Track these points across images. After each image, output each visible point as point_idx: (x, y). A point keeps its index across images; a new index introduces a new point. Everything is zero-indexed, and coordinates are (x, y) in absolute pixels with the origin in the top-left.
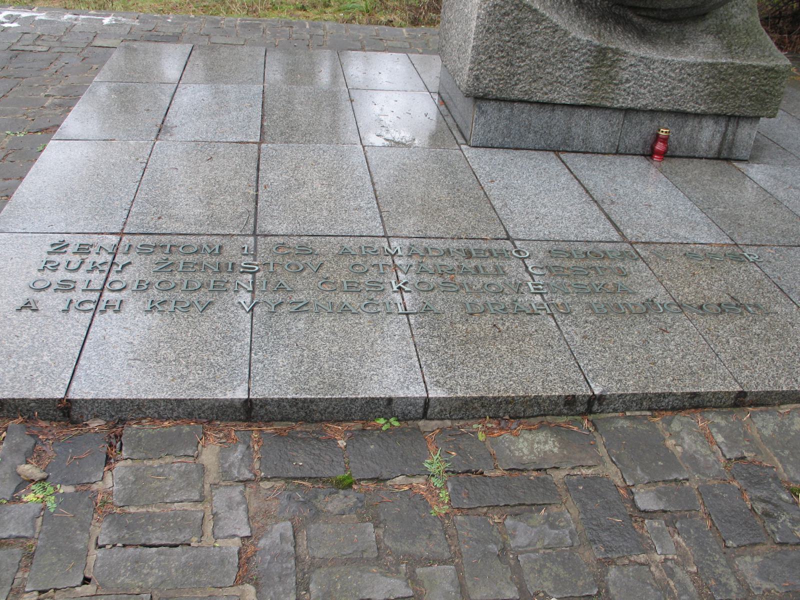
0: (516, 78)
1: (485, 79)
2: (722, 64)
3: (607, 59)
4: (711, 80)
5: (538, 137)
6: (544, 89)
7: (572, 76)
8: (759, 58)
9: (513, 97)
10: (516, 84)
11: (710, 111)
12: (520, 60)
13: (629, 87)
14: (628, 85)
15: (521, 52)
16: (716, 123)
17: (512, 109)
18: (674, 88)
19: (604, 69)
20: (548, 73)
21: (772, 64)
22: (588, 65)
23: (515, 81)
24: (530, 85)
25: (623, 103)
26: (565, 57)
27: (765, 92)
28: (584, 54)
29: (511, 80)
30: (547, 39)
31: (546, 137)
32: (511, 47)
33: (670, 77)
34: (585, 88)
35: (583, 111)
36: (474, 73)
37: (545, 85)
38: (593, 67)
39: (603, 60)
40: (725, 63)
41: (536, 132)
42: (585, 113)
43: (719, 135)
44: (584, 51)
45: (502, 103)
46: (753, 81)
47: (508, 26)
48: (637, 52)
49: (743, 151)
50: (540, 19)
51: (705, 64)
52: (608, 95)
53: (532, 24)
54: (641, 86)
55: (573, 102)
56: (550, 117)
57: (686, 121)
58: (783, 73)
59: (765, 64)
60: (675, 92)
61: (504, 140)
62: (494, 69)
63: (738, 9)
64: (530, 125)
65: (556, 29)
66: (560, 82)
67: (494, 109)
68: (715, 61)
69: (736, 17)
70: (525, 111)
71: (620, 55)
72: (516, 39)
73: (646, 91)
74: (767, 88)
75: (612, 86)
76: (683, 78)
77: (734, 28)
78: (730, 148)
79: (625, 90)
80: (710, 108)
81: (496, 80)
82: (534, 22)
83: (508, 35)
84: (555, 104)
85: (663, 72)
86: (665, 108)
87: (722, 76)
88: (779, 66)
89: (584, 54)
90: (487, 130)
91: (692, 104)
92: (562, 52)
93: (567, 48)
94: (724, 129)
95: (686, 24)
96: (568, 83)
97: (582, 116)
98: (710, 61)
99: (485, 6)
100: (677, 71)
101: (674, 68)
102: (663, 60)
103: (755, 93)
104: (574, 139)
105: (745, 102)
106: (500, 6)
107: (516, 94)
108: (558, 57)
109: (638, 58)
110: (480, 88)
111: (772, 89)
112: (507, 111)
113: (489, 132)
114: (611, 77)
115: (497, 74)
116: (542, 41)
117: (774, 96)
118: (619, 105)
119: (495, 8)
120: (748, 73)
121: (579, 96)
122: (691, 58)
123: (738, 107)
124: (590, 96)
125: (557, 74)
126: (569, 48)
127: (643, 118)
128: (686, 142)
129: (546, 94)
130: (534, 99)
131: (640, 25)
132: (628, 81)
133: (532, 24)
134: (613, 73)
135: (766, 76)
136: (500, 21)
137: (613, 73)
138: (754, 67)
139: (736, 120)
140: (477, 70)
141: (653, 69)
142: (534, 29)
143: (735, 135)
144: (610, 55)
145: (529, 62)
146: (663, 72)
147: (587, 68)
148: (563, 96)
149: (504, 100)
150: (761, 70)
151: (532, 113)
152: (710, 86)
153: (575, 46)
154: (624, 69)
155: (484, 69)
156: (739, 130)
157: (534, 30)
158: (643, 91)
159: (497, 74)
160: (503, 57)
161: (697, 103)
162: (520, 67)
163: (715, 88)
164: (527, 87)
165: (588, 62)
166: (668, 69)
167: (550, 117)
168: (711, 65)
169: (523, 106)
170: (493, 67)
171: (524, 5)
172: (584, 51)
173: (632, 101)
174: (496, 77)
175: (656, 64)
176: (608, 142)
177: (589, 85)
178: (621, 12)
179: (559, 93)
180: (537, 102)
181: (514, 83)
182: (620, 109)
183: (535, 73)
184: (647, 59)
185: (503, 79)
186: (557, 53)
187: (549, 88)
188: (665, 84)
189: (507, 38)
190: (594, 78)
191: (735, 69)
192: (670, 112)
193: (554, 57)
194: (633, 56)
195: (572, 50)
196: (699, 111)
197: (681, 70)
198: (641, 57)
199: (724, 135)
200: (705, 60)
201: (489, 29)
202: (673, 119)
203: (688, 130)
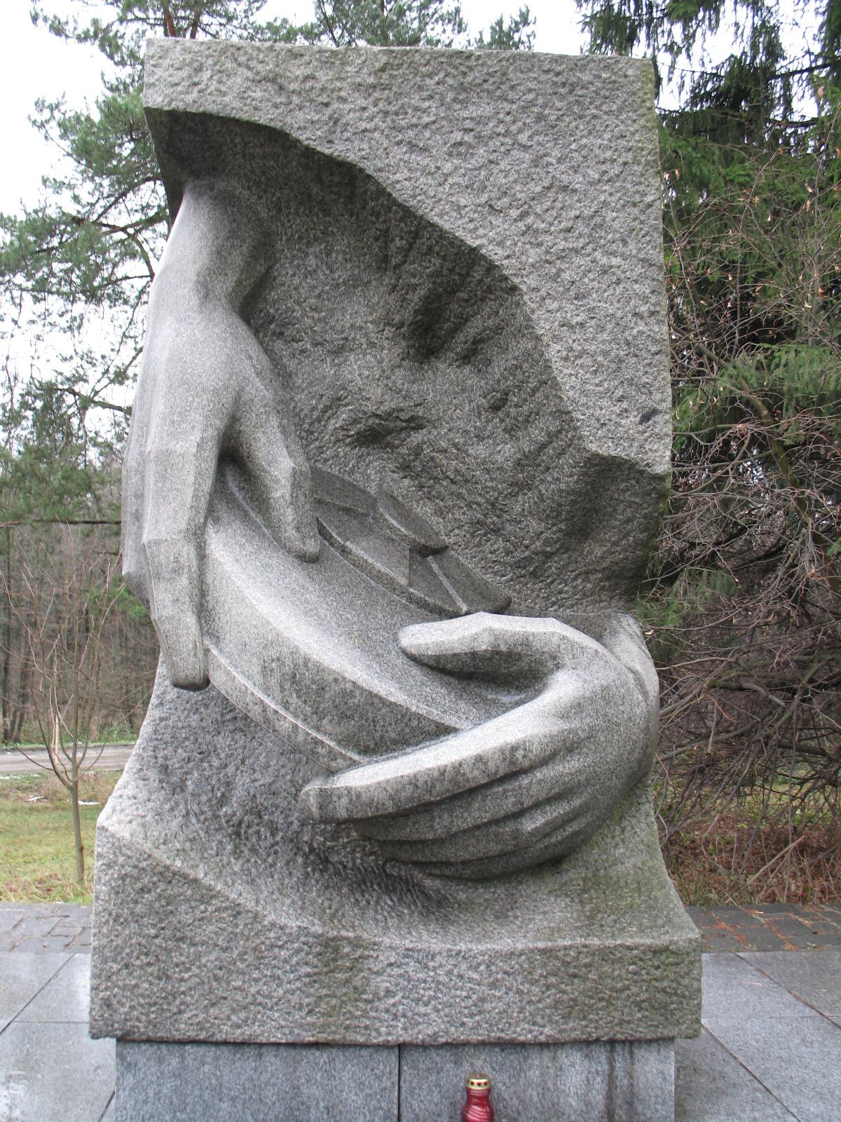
0: (178, 1002)
1: (123, 1005)
2: (566, 948)
3: (342, 958)
4: (552, 980)
5: (240, 1107)
6: (234, 1018)
7: (281, 992)
8: (641, 930)
9: (177, 1036)
10: (180, 1012)
11: (564, 1037)
12: (181, 967)
13: (394, 1005)
14: (391, 1001)
15: (181, 954)
16: (587, 1056)
17: (182, 1056)
18: (482, 1000)
19: (341, 976)
20: (235, 989)
21: (664, 940)
22: (308, 969)
23: (178, 1007)
24: (207, 1013)
25: (389, 1034)
26: (262, 958)
27: (664, 990)
28: (298, 951)
29: (169, 1004)
30: (223, 930)
31: (255, 1106)
32: (160, 947)
33: (471, 980)
34: (310, 1012)
35: (317, 1053)
36: (101, 995)
37: (233, 1010)
38: (319, 974)
39: (335, 960)
40: (571, 947)
41: (233, 1099)
42: (322, 1057)
43: (599, 1079)
44: (296, 945)
45: (163, 1047)
46: (636, 973)
47: (151, 911)
48: (398, 942)
49: (659, 1107)
50: (207, 896)
51: (532, 951)
52: (356, 1022)
53: (193, 904)
54: (417, 1001)
55: (290, 1039)
56: (255, 1069)
57: (526, 1059)
58: (688, 953)
59: (648, 941)
60: (487, 1006)
61: (174, 1116)
62: (136, 986)
63: (627, 849)
64: (221, 1085)
65: (237, 911)
66: (260, 1004)
67: (148, 1059)
68: (549, 944)
69: (622, 863)
70: (209, 1060)
71: (366, 948)
72: (168, 933)
73: (429, 1009)
74: (665, 984)
75: (361, 1004)
76: (497, 980)
77: (617, 883)
78: (630, 1104)
79: (387, 1011)
80: (564, 1031)
81: (142, 1006)
82: (196, 900)
83: (154, 925)
84: (261, 1045)
85: (455, 972)
86: (474, 1038)
87: (571, 970)
88: (676, 943)
89: (298, 951)
90: (141, 1098)
91: (526, 1026)
92: (255, 949)
93: (263, 943)
94: (606, 1067)
95: (521, 882)
96: (276, 1004)
97: (317, 1064)
98: (541, 945)
99: (107, 878)
100: (482, 968)
101: (474, 964)
102: (450, 950)
103: (644, 996)
104: (309, 1108)
105: (630, 1014)
106: (132, 876)
107: (184, 1029)
108: (250, 958)
109: (400, 951)
110: (114, 1022)
111: (674, 985)
112: (175, 1061)
113: (145, 1102)
114: (356, 988)
115: (142, 996)
116: (216, 933)
117: (684, 997)
118: (381, 1039)
119: (123, 880)
120: (620, 960)
121: (301, 1026)
122: (505, 943)
123: (620, 1024)
124: (323, 1026)
125: (253, 990)
126: (268, 942)
127: (438, 1059)
128: (535, 1099)
129: (239, 1026)
130: (219, 1037)
131: (438, 891)
132: (389, 993)
133: (193, 904)
134: (357, 981)
135: (656, 963)
136: (136, 902)
137: (357, 981)
138: (629, 948)
139: (627, 1049)
140: (106, 989)
141: (435, 968)
142: (197, 912)
143: (632, 1077)
144: (347, 950)
145: (197, 971)
146: (455, 972)
147: (308, 975)
148: (271, 1028)
149: (162, 1041)
150: (644, 952)
151: (221, 1063)
152: (553, 991)
153: (278, 938)
154: (377, 973)
155: (119, 987)
156: (637, 1066)
157: (198, 914)
158: (422, 1009)
159: (142, 996)
160: (149, 964)
161: (534, 1024)
162: (182, 980)
163: (563, 992)
164: (202, 1016)
165: (306, 964)
166: (464, 966)
167: (255, 1069)
168: (543, 952)
169: (202, 1050)
170: (133, 982)
171: (174, 874)
172: (296, 945)
173: (405, 1029)
174: (142, 1001)
175: (438, 959)
176: (376, 1109)
177: (317, 1004)
178: (403, 873)
179: (263, 1024)
180: (225, 1043)
181: (175, 1010)
182: (386, 1046)
183: (211, 991)
184: (419, 951)
185: (155, 1004)
186: (246, 953)
187: (243, 1015)
188: (464, 994)
189: (153, 932)
190: (325, 991)
191: (593, 955)
192: (483, 1044)
193: (243, 960)
194: (391, 947)
195: (273, 946)
196: (542, 1038)
197: (488, 966)
198: (407, 949)
199: (611, 1078)
200: (531, 945)
201: (118, 916)
202: (498, 1056)
203: (534, 1074)
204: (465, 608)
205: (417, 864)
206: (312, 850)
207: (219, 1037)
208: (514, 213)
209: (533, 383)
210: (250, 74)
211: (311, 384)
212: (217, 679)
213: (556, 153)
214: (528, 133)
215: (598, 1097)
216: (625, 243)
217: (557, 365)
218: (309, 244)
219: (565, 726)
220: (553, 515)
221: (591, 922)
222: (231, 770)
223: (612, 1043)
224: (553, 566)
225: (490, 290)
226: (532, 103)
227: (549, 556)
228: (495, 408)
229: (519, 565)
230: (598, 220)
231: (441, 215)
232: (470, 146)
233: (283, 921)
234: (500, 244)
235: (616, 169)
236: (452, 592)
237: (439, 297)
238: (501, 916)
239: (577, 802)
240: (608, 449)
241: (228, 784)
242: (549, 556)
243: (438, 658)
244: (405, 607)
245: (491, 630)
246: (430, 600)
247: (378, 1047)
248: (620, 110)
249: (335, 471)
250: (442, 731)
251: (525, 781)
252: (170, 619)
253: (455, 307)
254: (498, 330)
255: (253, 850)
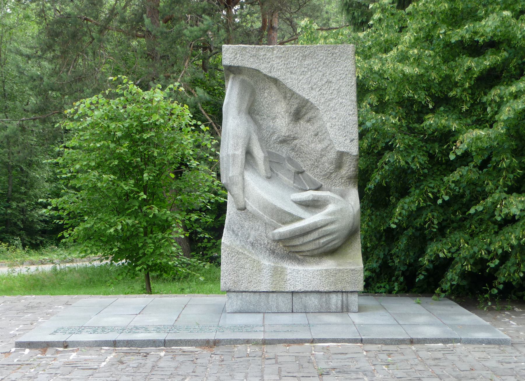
4: (327, 276)
41: (254, 305)
107: (242, 289)
112: (240, 297)
134: (282, 277)
168: (325, 270)
169: (246, 294)
180: (252, 292)
187: (256, 285)
196: (325, 290)
204: (308, 188)
205: (296, 252)
206: (271, 250)
207: (251, 290)
208: (318, 90)
209: (324, 132)
210: (249, 55)
211: (267, 128)
212: (248, 208)
213: (328, 73)
214: (321, 67)
215: (340, 303)
216: (346, 96)
217: (328, 128)
218: (265, 90)
219: (330, 217)
220: (331, 163)
221: (339, 265)
222: (249, 231)
223: (342, 292)
224: (333, 176)
225: (312, 108)
226: (322, 59)
227: (331, 173)
228: (316, 135)
229: (324, 175)
230: (339, 90)
231: (299, 90)
232: (306, 72)
233: (265, 263)
234: (314, 98)
235: (344, 76)
236: (305, 184)
237: (300, 108)
238: (291, 232)
239: (334, 236)
240: (342, 149)
241: (249, 234)
242: (331, 173)
243: (300, 202)
244: (293, 189)
245: (313, 195)
246: (299, 187)
247: (287, 292)
248: (345, 60)
249: (274, 151)
250: (300, 219)
251: (320, 230)
252: (237, 194)
253: (304, 110)
254: (315, 117)
255: (256, 249)
